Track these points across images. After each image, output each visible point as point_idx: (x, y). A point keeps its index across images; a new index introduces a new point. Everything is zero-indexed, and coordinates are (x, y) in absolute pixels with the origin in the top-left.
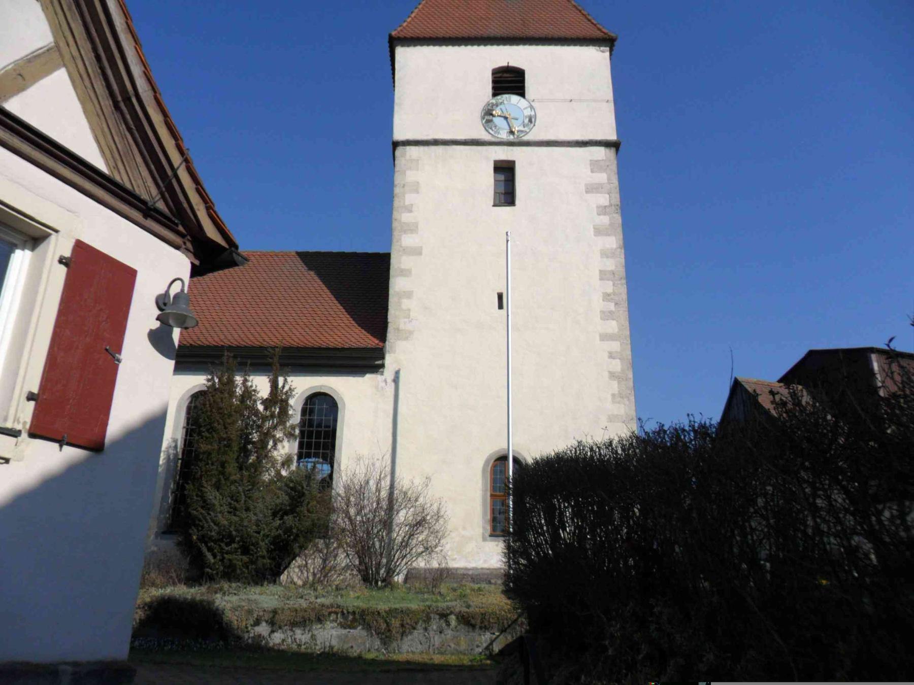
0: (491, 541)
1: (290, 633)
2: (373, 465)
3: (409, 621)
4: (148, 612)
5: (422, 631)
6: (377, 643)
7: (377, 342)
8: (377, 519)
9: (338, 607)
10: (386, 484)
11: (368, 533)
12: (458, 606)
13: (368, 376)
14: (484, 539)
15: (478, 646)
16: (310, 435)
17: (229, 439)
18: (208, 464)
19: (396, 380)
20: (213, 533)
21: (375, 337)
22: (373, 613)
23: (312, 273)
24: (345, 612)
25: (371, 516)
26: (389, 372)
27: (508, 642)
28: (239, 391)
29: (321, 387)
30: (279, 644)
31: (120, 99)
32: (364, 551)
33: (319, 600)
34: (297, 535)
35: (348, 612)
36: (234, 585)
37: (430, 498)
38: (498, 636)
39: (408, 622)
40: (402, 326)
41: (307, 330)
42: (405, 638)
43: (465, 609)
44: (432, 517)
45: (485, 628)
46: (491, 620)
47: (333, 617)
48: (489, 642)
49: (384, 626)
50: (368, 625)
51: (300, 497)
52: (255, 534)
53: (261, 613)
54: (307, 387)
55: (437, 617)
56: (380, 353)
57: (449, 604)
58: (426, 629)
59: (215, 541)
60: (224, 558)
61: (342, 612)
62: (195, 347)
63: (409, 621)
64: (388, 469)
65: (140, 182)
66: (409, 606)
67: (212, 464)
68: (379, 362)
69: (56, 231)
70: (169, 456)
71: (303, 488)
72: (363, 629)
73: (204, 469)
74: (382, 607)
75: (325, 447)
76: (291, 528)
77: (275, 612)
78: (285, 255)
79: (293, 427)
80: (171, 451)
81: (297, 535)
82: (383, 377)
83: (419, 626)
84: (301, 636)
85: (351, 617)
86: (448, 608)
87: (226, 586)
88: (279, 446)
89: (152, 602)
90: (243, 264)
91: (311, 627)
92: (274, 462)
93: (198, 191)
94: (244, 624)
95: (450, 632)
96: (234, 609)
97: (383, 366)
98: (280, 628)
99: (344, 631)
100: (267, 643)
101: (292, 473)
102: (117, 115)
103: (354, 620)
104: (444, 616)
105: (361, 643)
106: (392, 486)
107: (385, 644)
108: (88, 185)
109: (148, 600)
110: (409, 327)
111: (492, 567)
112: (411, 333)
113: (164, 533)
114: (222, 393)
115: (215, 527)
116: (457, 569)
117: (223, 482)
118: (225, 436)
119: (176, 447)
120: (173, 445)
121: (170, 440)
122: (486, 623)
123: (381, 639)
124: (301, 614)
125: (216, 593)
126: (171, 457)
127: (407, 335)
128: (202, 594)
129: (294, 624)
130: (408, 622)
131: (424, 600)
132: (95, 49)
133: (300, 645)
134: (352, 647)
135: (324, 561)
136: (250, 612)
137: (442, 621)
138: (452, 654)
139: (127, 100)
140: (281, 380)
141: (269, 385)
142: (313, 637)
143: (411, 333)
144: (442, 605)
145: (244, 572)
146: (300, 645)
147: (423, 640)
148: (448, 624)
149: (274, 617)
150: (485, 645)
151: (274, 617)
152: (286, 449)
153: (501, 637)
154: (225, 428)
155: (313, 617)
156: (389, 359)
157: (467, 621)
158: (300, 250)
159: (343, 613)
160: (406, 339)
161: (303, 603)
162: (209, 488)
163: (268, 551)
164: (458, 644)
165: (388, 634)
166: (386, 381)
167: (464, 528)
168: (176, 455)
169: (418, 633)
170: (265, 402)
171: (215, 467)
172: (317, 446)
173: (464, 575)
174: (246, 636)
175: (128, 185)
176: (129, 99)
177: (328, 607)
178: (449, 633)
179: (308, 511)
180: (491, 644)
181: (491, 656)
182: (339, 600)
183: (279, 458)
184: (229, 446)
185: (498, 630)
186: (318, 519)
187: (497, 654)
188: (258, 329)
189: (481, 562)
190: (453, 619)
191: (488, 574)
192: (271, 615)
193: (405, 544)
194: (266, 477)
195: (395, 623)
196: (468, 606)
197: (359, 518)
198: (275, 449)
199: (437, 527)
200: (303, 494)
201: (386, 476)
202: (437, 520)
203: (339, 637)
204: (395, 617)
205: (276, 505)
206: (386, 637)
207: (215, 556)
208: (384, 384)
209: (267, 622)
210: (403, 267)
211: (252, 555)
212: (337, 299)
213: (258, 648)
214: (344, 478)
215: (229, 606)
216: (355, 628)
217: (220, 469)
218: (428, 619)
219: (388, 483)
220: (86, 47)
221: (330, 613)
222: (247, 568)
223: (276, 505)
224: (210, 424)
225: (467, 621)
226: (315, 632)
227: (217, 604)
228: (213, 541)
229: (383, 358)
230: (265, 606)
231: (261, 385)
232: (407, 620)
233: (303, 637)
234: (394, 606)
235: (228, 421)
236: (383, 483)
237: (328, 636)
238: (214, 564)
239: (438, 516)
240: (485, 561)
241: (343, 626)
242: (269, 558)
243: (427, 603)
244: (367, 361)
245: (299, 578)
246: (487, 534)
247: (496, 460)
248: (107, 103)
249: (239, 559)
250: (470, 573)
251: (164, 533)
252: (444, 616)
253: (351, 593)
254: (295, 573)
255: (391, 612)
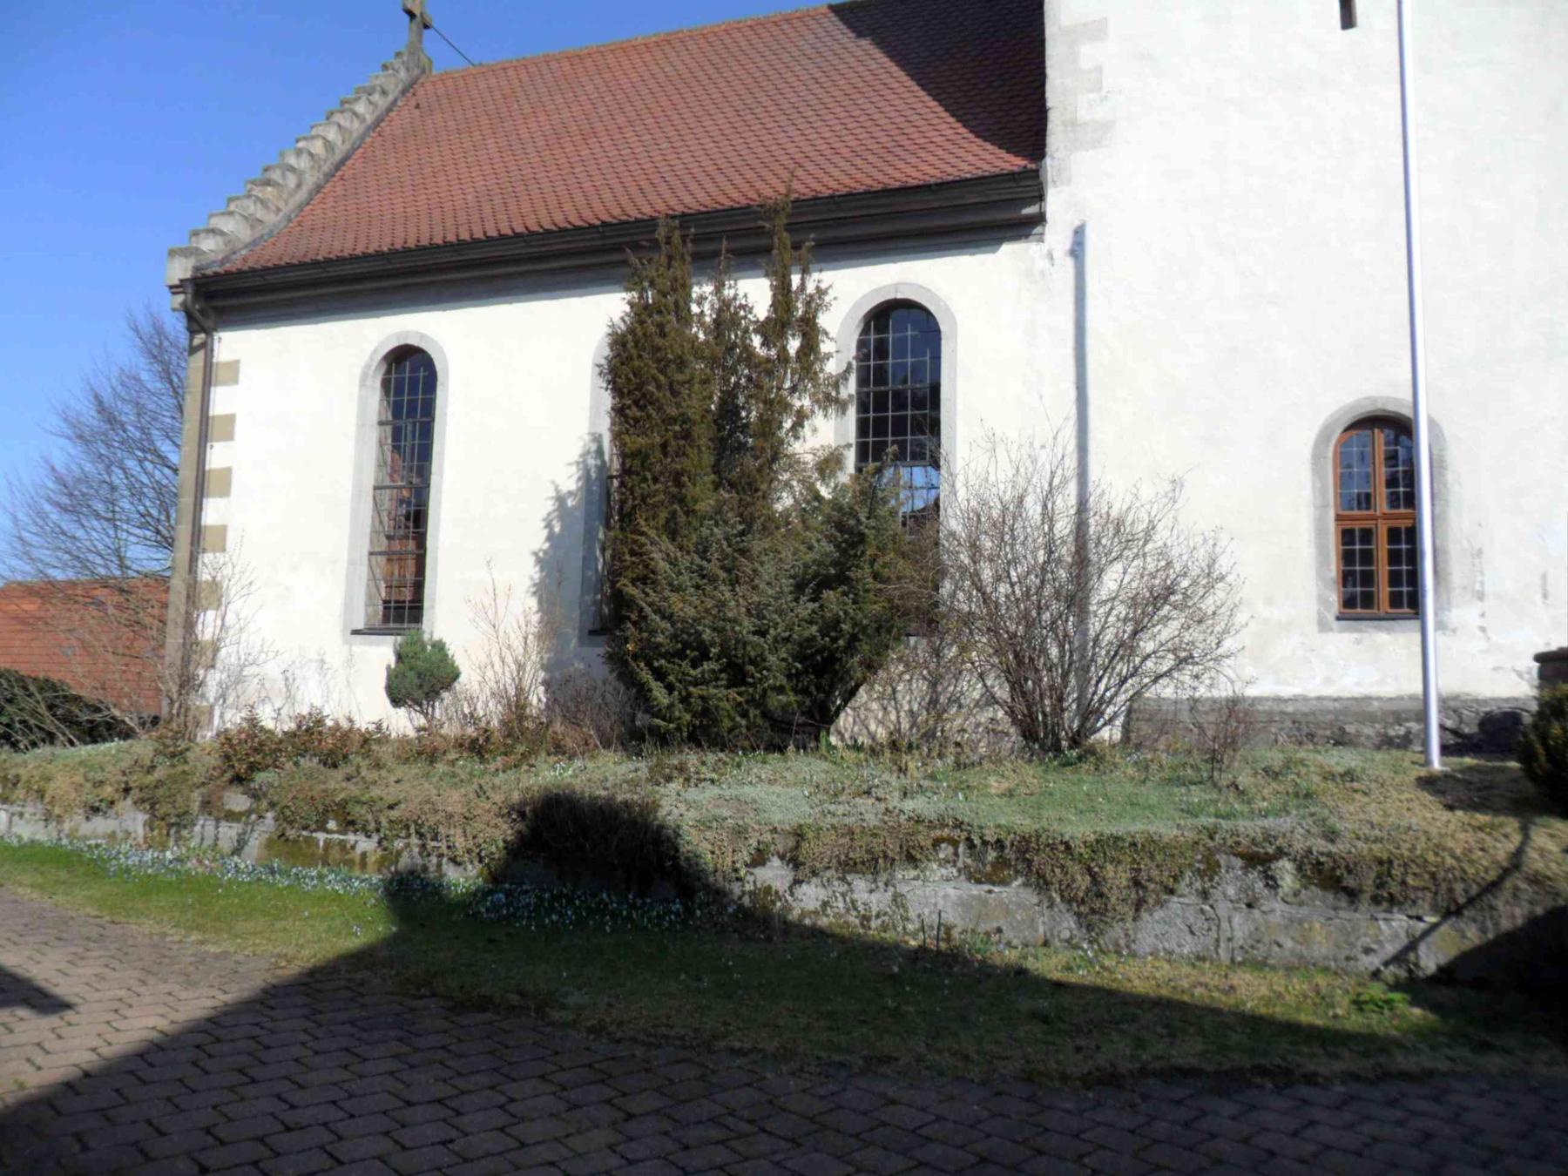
0: (1342, 631)
1: (840, 888)
2: (1034, 461)
3: (1154, 873)
4: (520, 826)
5: (1193, 899)
6: (1068, 924)
7: (1024, 163)
8: (1048, 590)
9: (959, 825)
10: (1066, 502)
11: (1030, 626)
12: (1294, 829)
13: (1006, 248)
14: (1323, 627)
15: (1368, 951)
16: (881, 404)
17: (685, 420)
18: (645, 480)
19: (1077, 251)
20: (660, 639)
21: (1016, 154)
22: (1053, 847)
23: (864, 42)
24: (977, 841)
25: (1033, 580)
26: (1057, 232)
27: (1467, 945)
28: (708, 312)
29: (896, 286)
30: (816, 912)
32: (1019, 664)
33: (909, 805)
34: (854, 638)
35: (985, 843)
36: (711, 758)
37: (1184, 533)
38: (1434, 927)
39: (1151, 874)
40: (1083, 114)
41: (858, 162)
42: (1145, 915)
43: (1319, 845)
44: (1194, 583)
45: (1387, 899)
46: (1410, 881)
47: (945, 851)
48: (1404, 941)
49: (1083, 882)
50: (1040, 876)
51: (853, 545)
52: (756, 638)
53: (767, 837)
54: (866, 289)
55: (1238, 862)
56: (1030, 187)
57: (1269, 822)
58: (1205, 895)
59: (668, 656)
60: (689, 695)
61: (969, 839)
62: (611, 224)
63: (1154, 873)
64: (1071, 462)
66: (1152, 829)
67: (656, 480)
68: (1031, 210)
70: (587, 472)
71: (858, 521)
72: (1025, 885)
73: (638, 492)
74: (1079, 830)
75: (918, 428)
76: (837, 621)
77: (799, 834)
79: (837, 382)
80: (592, 462)
81: (854, 638)
82: (1044, 247)
83: (1182, 887)
84: (867, 895)
85: (992, 855)
86: (1268, 837)
87: (692, 758)
88: (806, 431)
89: (524, 803)
91: (892, 876)
92: (794, 463)
94: (729, 861)
95: (1279, 906)
96: (703, 825)
97: (1040, 219)
98: (814, 873)
99: (977, 890)
100: (788, 908)
101: (840, 490)
103: (1001, 863)
104: (1258, 860)
105: (1017, 926)
106: (1082, 506)
107: (1090, 928)
109: (516, 797)
111: (1347, 695)
112: (1106, 127)
113: (592, 632)
114: (660, 312)
115: (665, 625)
116: (1256, 700)
117: (682, 519)
118: (673, 412)
119: (600, 452)
120: (594, 447)
121: (587, 438)
122: (1395, 888)
123: (1079, 915)
124: (861, 842)
125: (669, 779)
126: (593, 475)
127: (1101, 133)
128: (634, 784)
129: (848, 867)
130: (1151, 874)
131: (1191, 812)
133: (865, 919)
134: (999, 930)
135: (933, 685)
136: (740, 832)
137: (1253, 875)
138: (1290, 969)
140: (796, 280)
141: (770, 294)
142: (898, 900)
143: (1106, 127)
144: (1250, 828)
145: (738, 726)
146: (865, 919)
147: (1199, 924)
148: (1272, 883)
149: (797, 847)
150: (1391, 949)
151: (797, 847)
152: (825, 434)
153: (1444, 928)
154: (674, 393)
155: (893, 849)
156: (1056, 203)
157: (1330, 878)
159: (971, 845)
160: (1096, 144)
161: (869, 812)
162: (652, 533)
163: (789, 677)
164: (1305, 940)
165: (1097, 905)
166: (1050, 256)
167: (1269, 601)
168: (602, 468)
169: (1183, 906)
170: (763, 328)
171: (658, 486)
172: (900, 427)
173: (1270, 713)
174: (736, 889)
177: (931, 826)
178: (1276, 909)
179: (876, 576)
180: (1412, 946)
181: (1415, 987)
182: (961, 807)
183: (809, 458)
184: (687, 435)
185: (1435, 909)
186: (901, 597)
187: (1432, 980)
188: (750, 175)
189: (1318, 680)
190: (1286, 872)
191: (1337, 713)
192: (791, 842)
193: (1125, 648)
194: (784, 502)
195: (1117, 877)
196: (1331, 835)
197: (1003, 588)
198: (797, 438)
199: (1208, 605)
200: (862, 538)
201: (1064, 481)
202: (1210, 587)
203: (963, 904)
204: (1117, 862)
205: (806, 566)
206: (1092, 909)
207: (670, 688)
208: (1045, 264)
209: (782, 857)
211: (753, 685)
213: (760, 921)
214: (962, 494)
215: (691, 816)
216: (1004, 882)
217: (674, 490)
218: (1210, 869)
219: (1073, 500)
221: (937, 843)
222: (745, 715)
223: (806, 566)
224: (639, 387)
225: (1330, 878)
226: (903, 889)
227: (661, 813)
228: (664, 656)
229: (1040, 197)
230: (776, 817)
231: (755, 293)
232: (1149, 869)
233: (874, 898)
234: (1109, 829)
235: (679, 377)
236: (1059, 501)
237: (934, 901)
238: (671, 705)
239: (1211, 577)
240: (1328, 681)
241: (974, 877)
242: (796, 691)
243: (1207, 821)
244: (998, 209)
245: (880, 722)
246: (1331, 617)
247: (1348, 429)
249: (724, 697)
250: (1290, 709)
251: (592, 632)
252: (1258, 860)
253: (992, 780)
254: (866, 716)
255: (1102, 845)
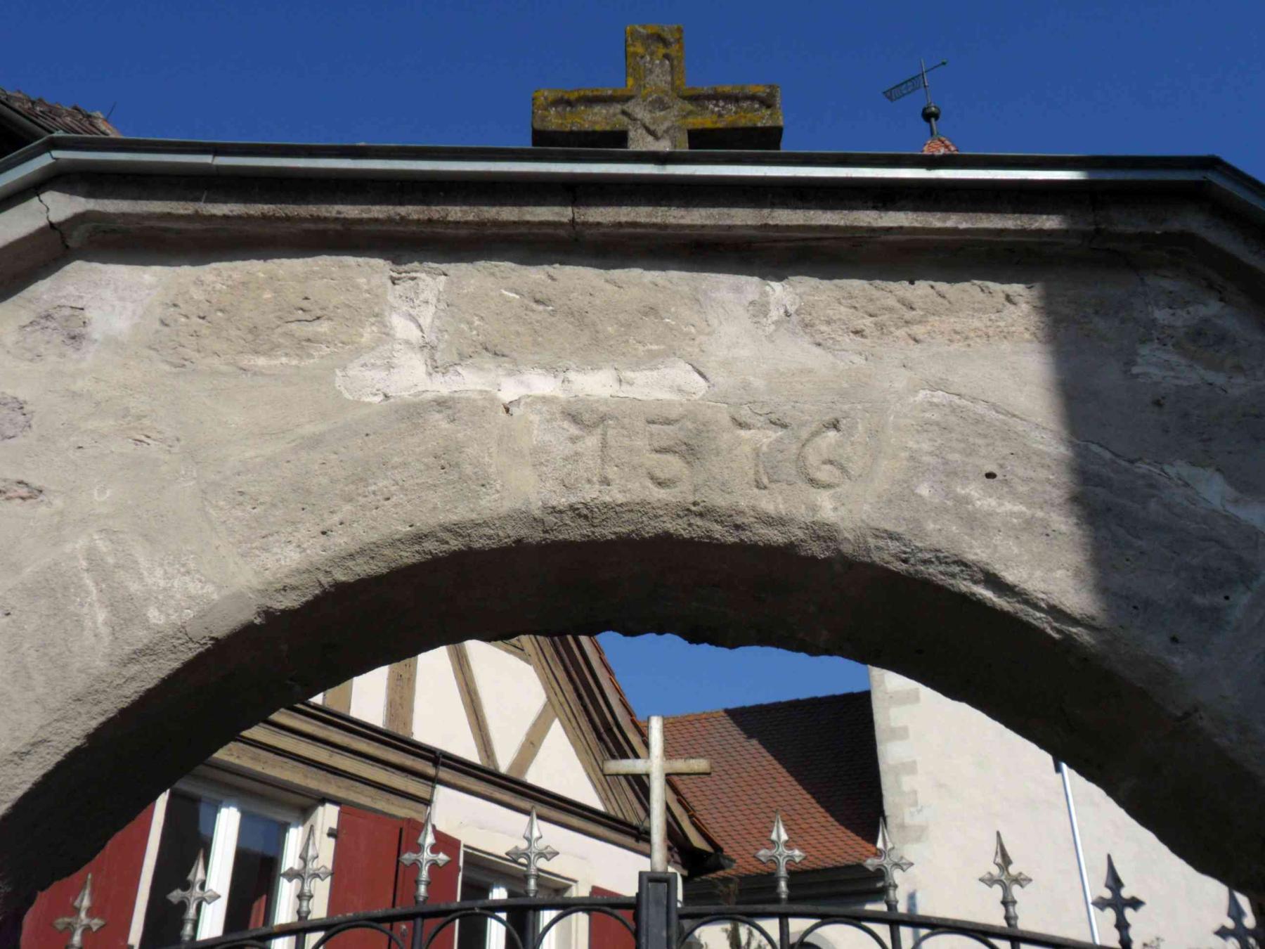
23: (754, 742)
31: (602, 730)
40: (908, 821)
65: (628, 806)
68: (880, 885)
69: (575, 881)
78: (706, 718)
90: (730, 866)
93: (679, 801)
102: (601, 746)
108: (575, 821)
110: (918, 820)
132: (576, 690)
139: (609, 730)
158: (731, 706)
160: (918, 839)
175: (620, 816)
176: (611, 730)
210: (893, 724)
212: (800, 782)
220: (568, 688)
248: (591, 737)
